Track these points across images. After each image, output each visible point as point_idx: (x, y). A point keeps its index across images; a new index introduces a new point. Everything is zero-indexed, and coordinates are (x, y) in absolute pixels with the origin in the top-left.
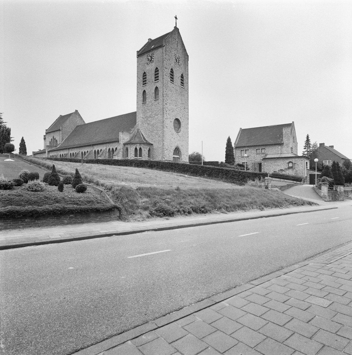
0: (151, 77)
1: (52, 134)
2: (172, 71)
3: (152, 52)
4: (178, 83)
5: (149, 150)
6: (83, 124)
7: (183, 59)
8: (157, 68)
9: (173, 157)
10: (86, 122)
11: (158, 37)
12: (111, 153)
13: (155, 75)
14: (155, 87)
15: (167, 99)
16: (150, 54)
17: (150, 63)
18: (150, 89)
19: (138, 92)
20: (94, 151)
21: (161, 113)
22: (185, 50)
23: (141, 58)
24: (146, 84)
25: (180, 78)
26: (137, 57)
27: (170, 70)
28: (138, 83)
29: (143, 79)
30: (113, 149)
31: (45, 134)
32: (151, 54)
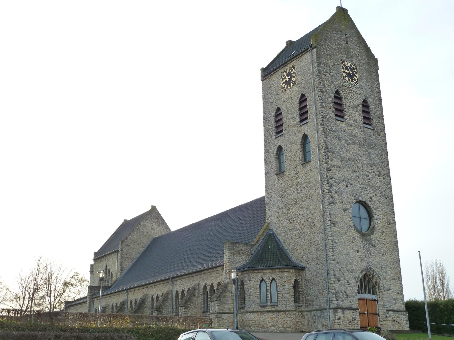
2: (338, 96)
3: (291, 65)
4: (355, 121)
5: (296, 284)
6: (164, 232)
7: (365, 67)
8: (303, 96)
9: (359, 299)
11: (363, 36)
12: (209, 295)
14: (301, 135)
17: (287, 87)
18: (291, 141)
19: (266, 151)
21: (317, 191)
22: (367, 49)
25: (360, 108)
26: (262, 80)
27: (332, 95)
28: (266, 131)
30: (212, 285)
31: (92, 262)
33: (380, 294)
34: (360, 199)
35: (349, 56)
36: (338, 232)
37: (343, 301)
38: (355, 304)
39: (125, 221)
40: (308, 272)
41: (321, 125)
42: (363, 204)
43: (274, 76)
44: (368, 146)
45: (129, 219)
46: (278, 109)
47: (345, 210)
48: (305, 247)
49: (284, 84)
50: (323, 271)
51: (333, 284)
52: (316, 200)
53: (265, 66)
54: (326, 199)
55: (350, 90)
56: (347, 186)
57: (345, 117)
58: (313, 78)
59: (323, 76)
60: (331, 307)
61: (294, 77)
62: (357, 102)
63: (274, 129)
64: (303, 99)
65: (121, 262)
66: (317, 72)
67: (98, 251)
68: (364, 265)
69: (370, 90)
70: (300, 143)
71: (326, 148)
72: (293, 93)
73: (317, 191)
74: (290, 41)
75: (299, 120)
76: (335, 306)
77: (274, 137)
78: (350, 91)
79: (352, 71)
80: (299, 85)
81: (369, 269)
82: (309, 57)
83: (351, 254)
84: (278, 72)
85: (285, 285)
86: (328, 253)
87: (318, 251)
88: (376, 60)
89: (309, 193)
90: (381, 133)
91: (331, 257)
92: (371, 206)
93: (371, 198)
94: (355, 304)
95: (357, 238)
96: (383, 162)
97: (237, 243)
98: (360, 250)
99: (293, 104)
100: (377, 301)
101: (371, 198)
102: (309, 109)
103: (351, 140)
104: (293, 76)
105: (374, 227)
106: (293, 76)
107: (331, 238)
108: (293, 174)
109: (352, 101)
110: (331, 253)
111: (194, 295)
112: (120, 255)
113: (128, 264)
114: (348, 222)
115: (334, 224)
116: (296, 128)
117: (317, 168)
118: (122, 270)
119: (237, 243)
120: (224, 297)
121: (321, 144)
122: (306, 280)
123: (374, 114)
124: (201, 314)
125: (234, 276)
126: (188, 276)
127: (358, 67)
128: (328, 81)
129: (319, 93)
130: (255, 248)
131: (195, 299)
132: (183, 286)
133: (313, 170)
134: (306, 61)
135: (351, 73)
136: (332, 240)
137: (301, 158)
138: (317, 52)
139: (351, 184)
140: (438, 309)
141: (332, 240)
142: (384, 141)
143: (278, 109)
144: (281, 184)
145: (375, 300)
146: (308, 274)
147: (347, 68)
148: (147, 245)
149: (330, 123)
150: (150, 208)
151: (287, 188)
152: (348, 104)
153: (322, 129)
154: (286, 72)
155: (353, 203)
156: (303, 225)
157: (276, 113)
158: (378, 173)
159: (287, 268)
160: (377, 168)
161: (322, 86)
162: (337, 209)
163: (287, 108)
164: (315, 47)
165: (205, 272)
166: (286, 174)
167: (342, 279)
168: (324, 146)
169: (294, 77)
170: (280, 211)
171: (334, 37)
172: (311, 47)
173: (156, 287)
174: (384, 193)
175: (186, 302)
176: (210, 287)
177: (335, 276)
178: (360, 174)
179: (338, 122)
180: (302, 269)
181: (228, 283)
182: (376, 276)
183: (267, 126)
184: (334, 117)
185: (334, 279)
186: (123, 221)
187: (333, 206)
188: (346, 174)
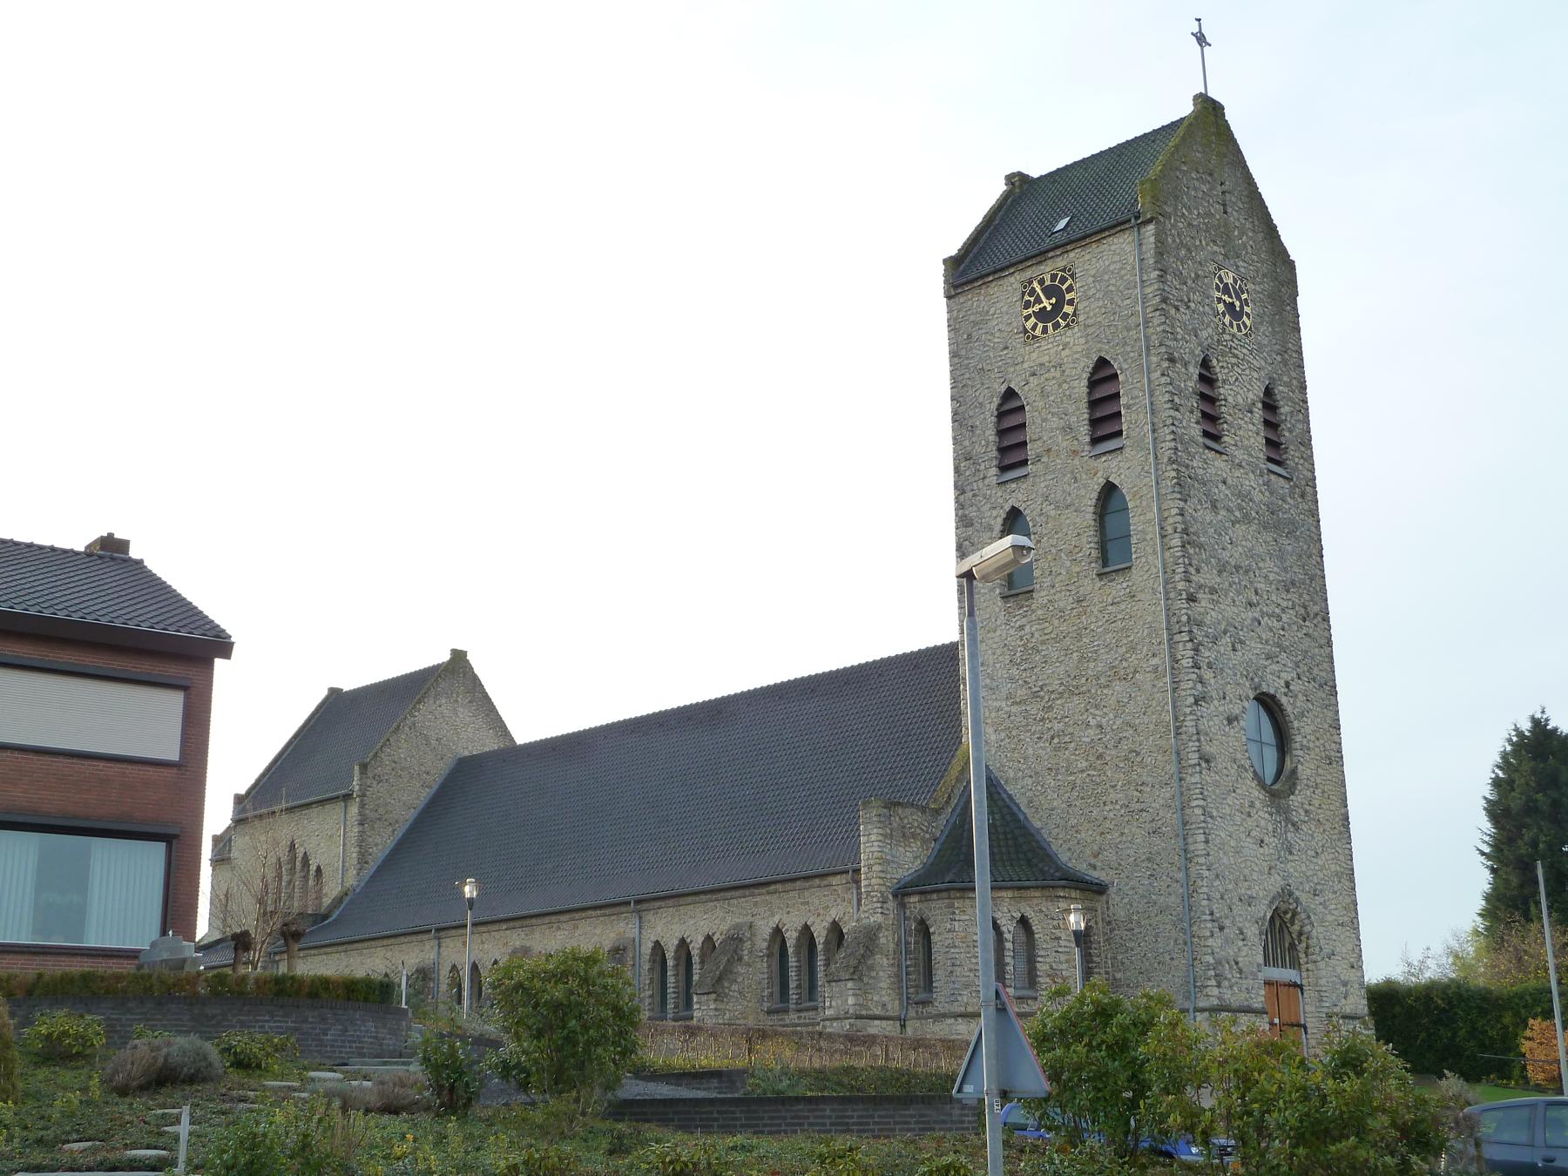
0: (1057, 418)
1: (285, 829)
6: (491, 744)
9: (1268, 983)
10: (525, 731)
13: (1093, 404)
15: (1195, 562)
16: (1046, 270)
17: (1045, 330)
20: (647, 948)
21: (1155, 661)
23: (976, 300)
24: (1024, 463)
25: (1258, 413)
26: (949, 297)
27: (1195, 371)
28: (964, 461)
29: (1001, 433)
32: (1054, 277)
33: (1310, 966)
34: (1265, 688)
35: (1232, 253)
36: (1217, 785)
37: (1231, 987)
38: (1259, 999)
39: (335, 694)
40: (1118, 899)
41: (1171, 461)
42: (1268, 703)
43: (994, 289)
44: (1277, 527)
45: (347, 686)
46: (1010, 394)
47: (1231, 720)
48: (1107, 824)
49: (1033, 320)
50: (1173, 898)
51: (1206, 938)
52: (1148, 686)
53: (953, 251)
54: (1184, 685)
55: (1236, 356)
56: (1234, 650)
57: (1226, 439)
58: (1144, 313)
59: (1173, 311)
60: (1201, 1004)
61: (1071, 302)
62: (1251, 395)
63: (995, 453)
64: (1102, 374)
65: (361, 833)
66: (1158, 299)
67: (249, 792)
68: (1275, 883)
69: (1279, 358)
70: (1091, 509)
71: (1185, 531)
72: (1067, 352)
73: (1155, 661)
74: (1020, 174)
75: (1088, 439)
76: (1216, 1002)
77: (994, 480)
78: (1234, 360)
79: (1239, 298)
80: (1090, 330)
81: (1286, 893)
82: (1128, 249)
83: (1246, 851)
84: (1012, 279)
85: (1059, 938)
86: (1192, 848)
87: (1155, 839)
88: (1291, 266)
89: (1125, 664)
90: (1306, 490)
91: (1202, 860)
92: (1289, 709)
93: (1287, 685)
94: (1259, 999)
95: (1257, 804)
96: (1312, 579)
97: (899, 804)
98: (1266, 839)
99: (1065, 386)
100: (1301, 987)
101: (1287, 685)
102: (1128, 407)
103: (1240, 509)
104: (1068, 297)
105: (1294, 771)
106: (1068, 297)
107: (1201, 803)
108: (1065, 602)
109: (1240, 392)
110: (1202, 846)
111: (740, 959)
112: (354, 810)
113: (383, 842)
114: (1239, 756)
115: (1207, 761)
116: (1077, 462)
117: (1154, 592)
118: (363, 860)
119: (899, 804)
120: (871, 968)
121: (1171, 520)
122: (1109, 923)
123: (1291, 431)
124: (762, 1016)
125: (1078, 923)
126: (702, 897)
127: (1250, 286)
128: (1184, 326)
129: (1165, 364)
130: (942, 820)
131: (741, 969)
132: (671, 928)
133: (1139, 596)
134: (1117, 258)
135: (1237, 304)
136: (1203, 808)
137: (1095, 553)
138: (1157, 235)
139: (1242, 642)
140: (1398, 1009)
141: (1203, 808)
142: (1314, 514)
143: (1010, 394)
144: (1022, 628)
145: (1295, 985)
146: (1117, 905)
147: (1226, 290)
148: (439, 780)
149: (1192, 457)
150: (446, 657)
151: (1043, 643)
152: (1230, 399)
153: (1174, 474)
154: (1041, 282)
155: (1247, 698)
156: (1100, 757)
157: (1000, 405)
158: (1302, 611)
159: (1064, 887)
160: (1301, 596)
161: (1171, 343)
162: (1212, 714)
163: (1044, 394)
164: (1150, 221)
165: (779, 887)
166: (1041, 597)
167: (1227, 923)
168: (1180, 527)
169: (1071, 302)
170: (1014, 709)
171: (1195, 189)
172: (1137, 218)
173: (564, 926)
174: (1316, 671)
175: (720, 980)
176: (795, 935)
177: (1212, 914)
178: (1263, 614)
179: (1211, 455)
180: (1099, 889)
181: (880, 927)
182: (1303, 916)
183: (967, 443)
184: (1201, 440)
185: (1209, 925)
186: (325, 693)
187: (1204, 709)
188: (1230, 611)
